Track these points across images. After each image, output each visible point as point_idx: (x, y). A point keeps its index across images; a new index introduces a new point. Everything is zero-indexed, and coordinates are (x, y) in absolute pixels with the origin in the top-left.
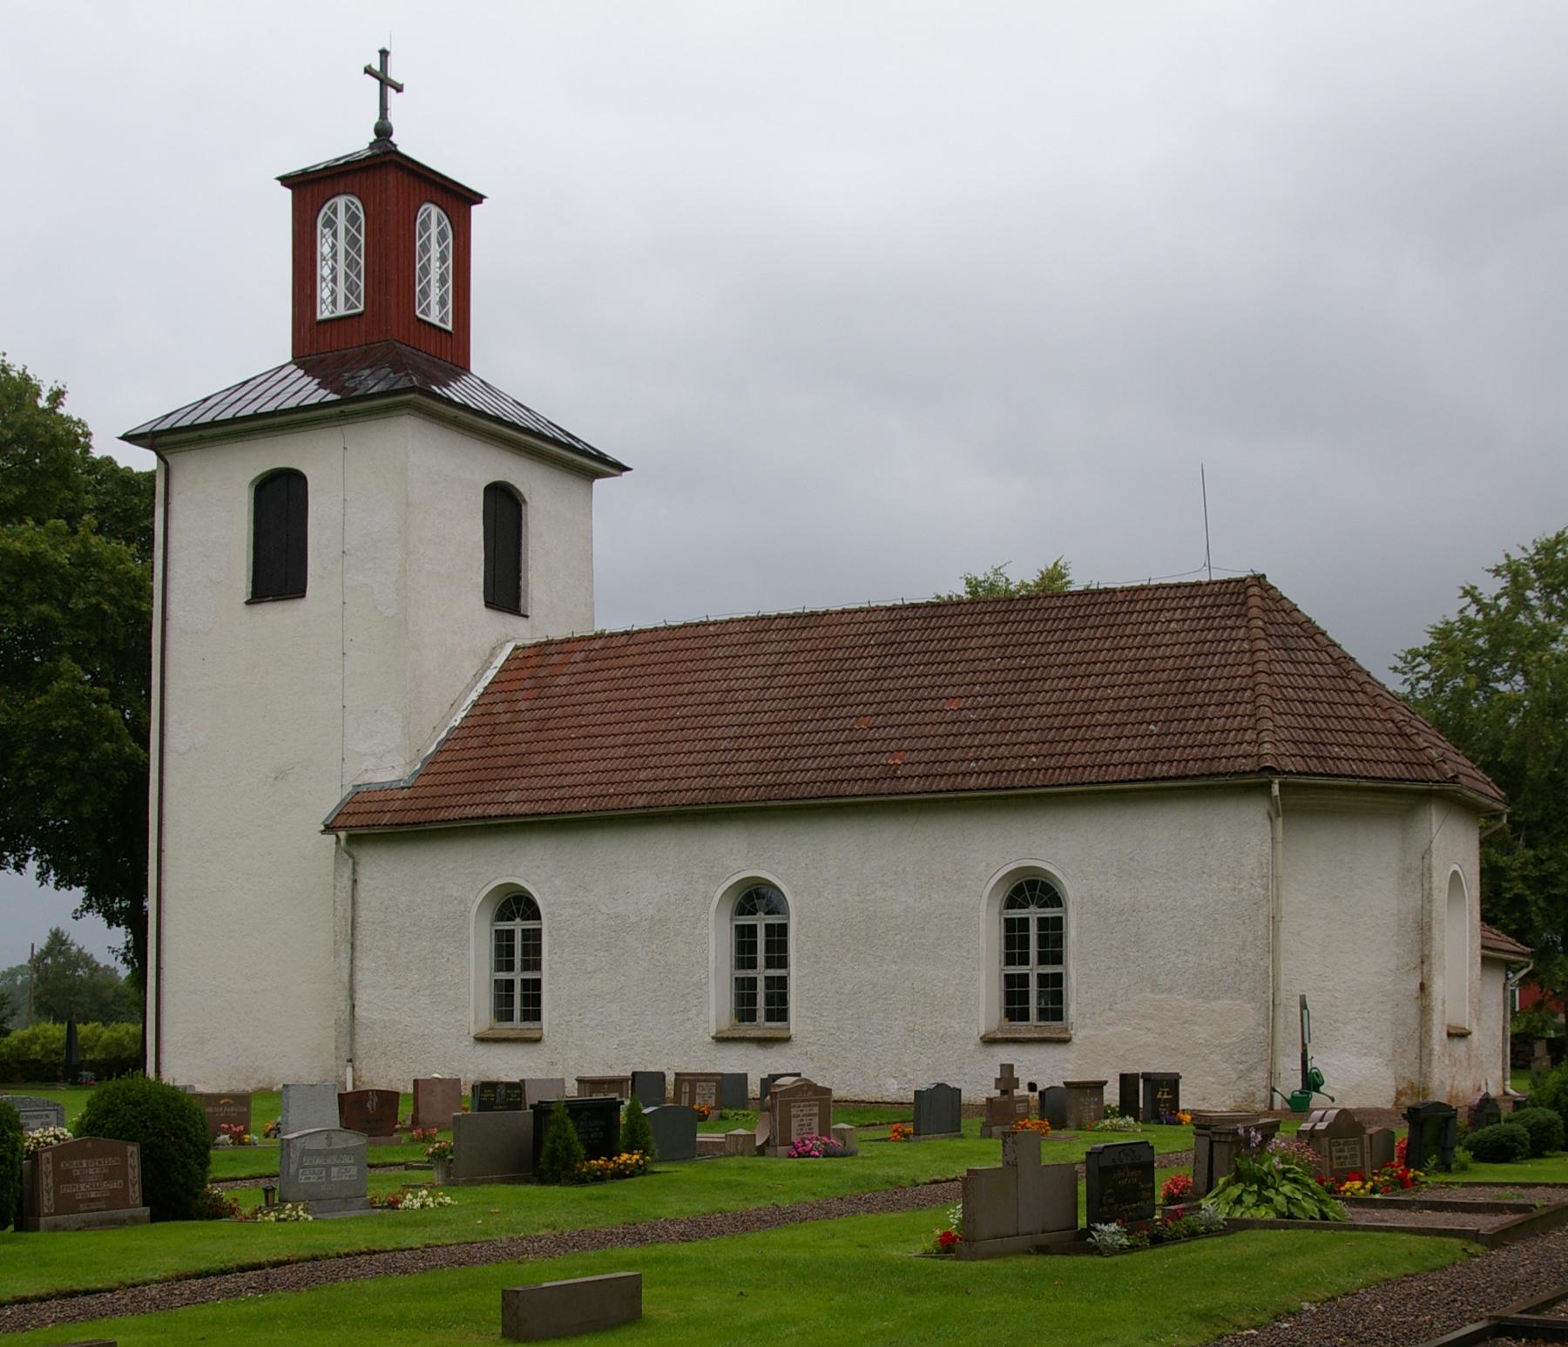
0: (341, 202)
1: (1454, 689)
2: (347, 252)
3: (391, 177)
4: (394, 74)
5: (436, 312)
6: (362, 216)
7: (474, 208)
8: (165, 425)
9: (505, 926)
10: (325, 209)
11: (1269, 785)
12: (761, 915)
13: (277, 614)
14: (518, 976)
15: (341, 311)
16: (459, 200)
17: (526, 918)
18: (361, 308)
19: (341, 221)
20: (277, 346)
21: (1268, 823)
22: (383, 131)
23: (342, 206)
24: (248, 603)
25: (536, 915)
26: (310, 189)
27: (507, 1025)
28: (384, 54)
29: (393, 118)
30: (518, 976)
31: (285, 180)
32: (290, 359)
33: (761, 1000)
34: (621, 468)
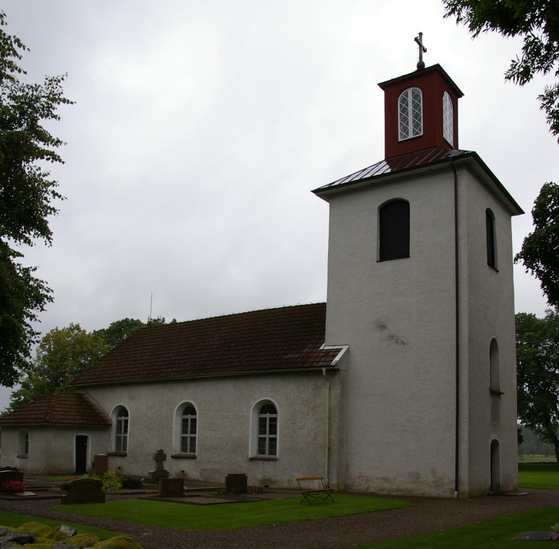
0: (410, 91)
4: (425, 44)
5: (450, 140)
6: (421, 95)
7: (459, 99)
9: (263, 416)
10: (402, 95)
12: (123, 417)
13: (392, 266)
14: (268, 436)
15: (411, 136)
16: (456, 93)
17: (271, 413)
18: (422, 134)
19: (410, 99)
20: (380, 154)
23: (410, 93)
24: (377, 262)
25: (275, 412)
26: (393, 88)
27: (184, 453)
28: (421, 34)
30: (268, 436)
31: (383, 85)
32: (384, 158)
33: (267, 446)
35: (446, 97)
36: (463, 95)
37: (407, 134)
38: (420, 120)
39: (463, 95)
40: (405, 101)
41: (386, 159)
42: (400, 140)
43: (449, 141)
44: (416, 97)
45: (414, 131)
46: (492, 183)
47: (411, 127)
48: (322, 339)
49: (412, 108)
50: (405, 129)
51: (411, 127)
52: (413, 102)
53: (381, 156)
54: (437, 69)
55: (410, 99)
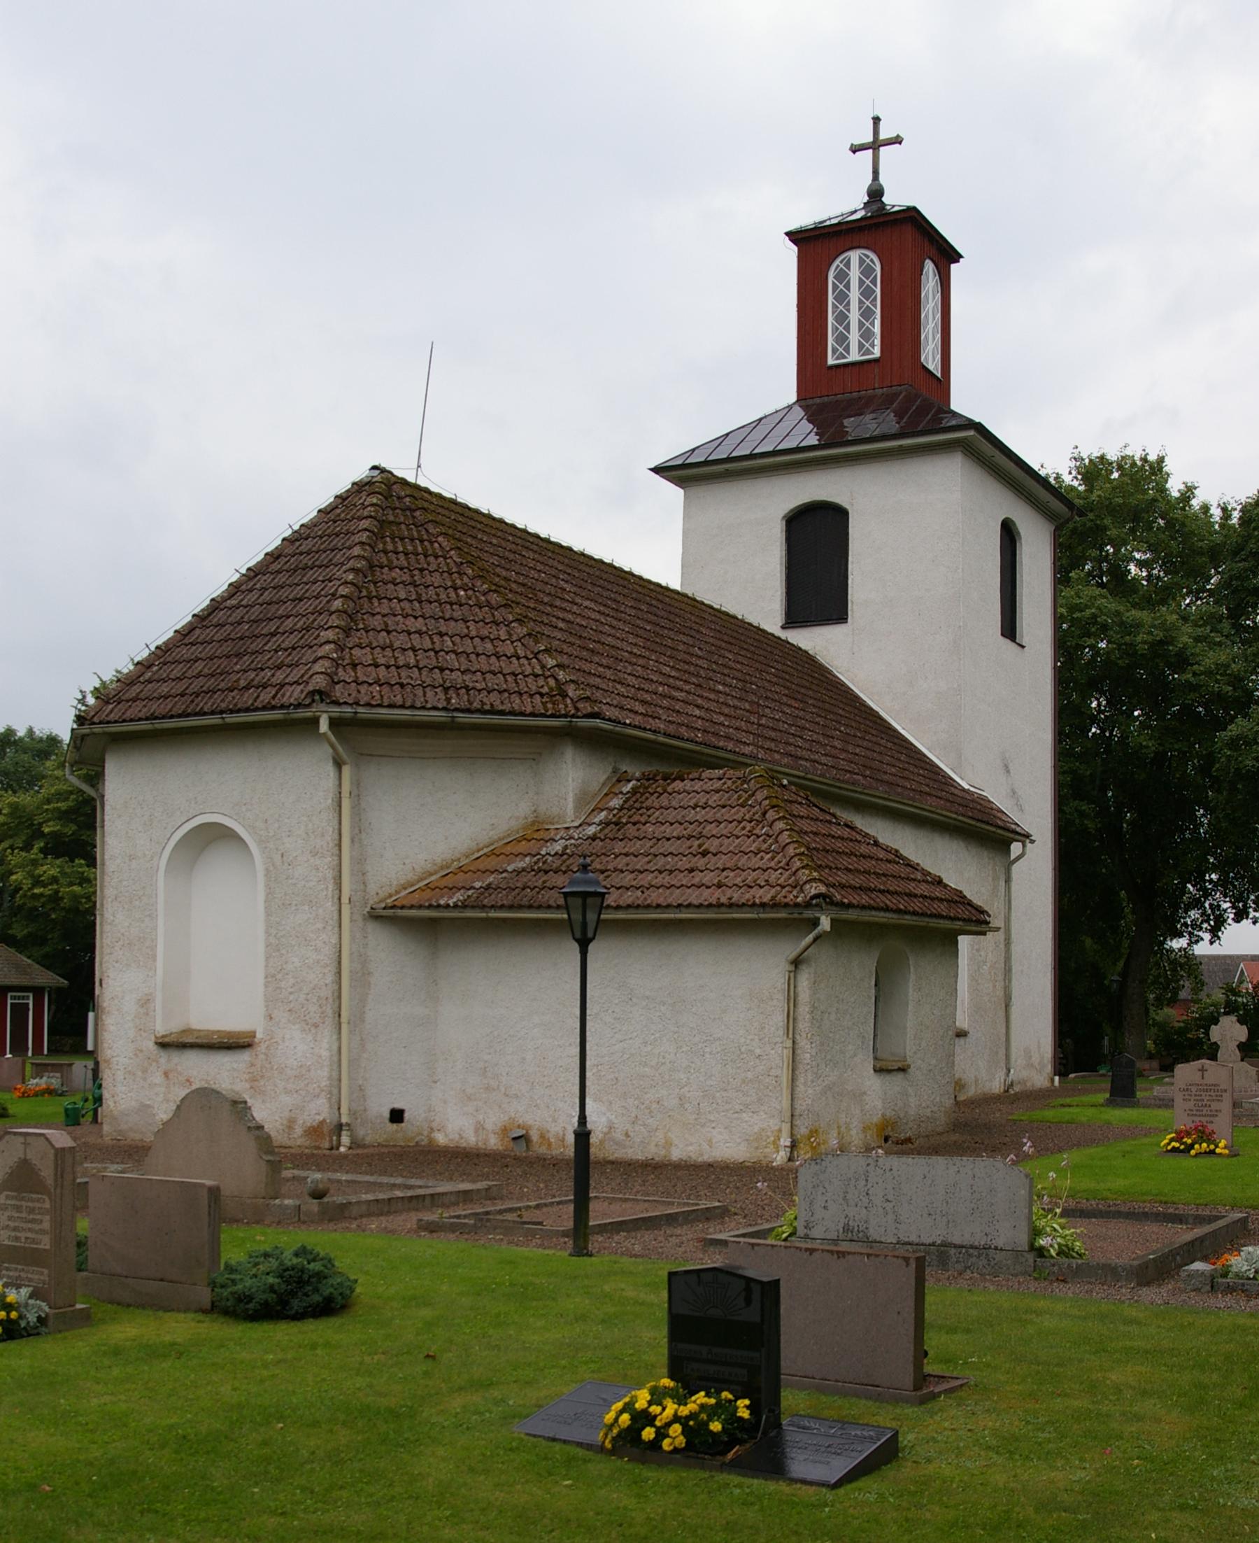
0: (854, 256)
1: (1130, 823)
2: (861, 302)
3: (909, 233)
5: (933, 365)
7: (953, 266)
8: (721, 454)
10: (837, 262)
11: (315, 721)
15: (854, 356)
16: (947, 255)
19: (855, 274)
20: (782, 387)
21: (330, 768)
22: (876, 193)
26: (817, 245)
29: (882, 180)
34: (657, 470)
35: (929, 267)
36: (961, 257)
37: (847, 349)
38: (874, 282)
39: (961, 257)
40: (842, 276)
41: (801, 399)
42: (831, 361)
43: (931, 367)
44: (867, 271)
45: (861, 346)
46: (1011, 466)
47: (854, 337)
48: (61, 742)
49: (858, 273)
50: (842, 339)
51: (854, 337)
52: (861, 282)
53: (789, 394)
54: (912, 218)
55: (855, 274)
